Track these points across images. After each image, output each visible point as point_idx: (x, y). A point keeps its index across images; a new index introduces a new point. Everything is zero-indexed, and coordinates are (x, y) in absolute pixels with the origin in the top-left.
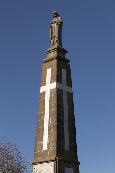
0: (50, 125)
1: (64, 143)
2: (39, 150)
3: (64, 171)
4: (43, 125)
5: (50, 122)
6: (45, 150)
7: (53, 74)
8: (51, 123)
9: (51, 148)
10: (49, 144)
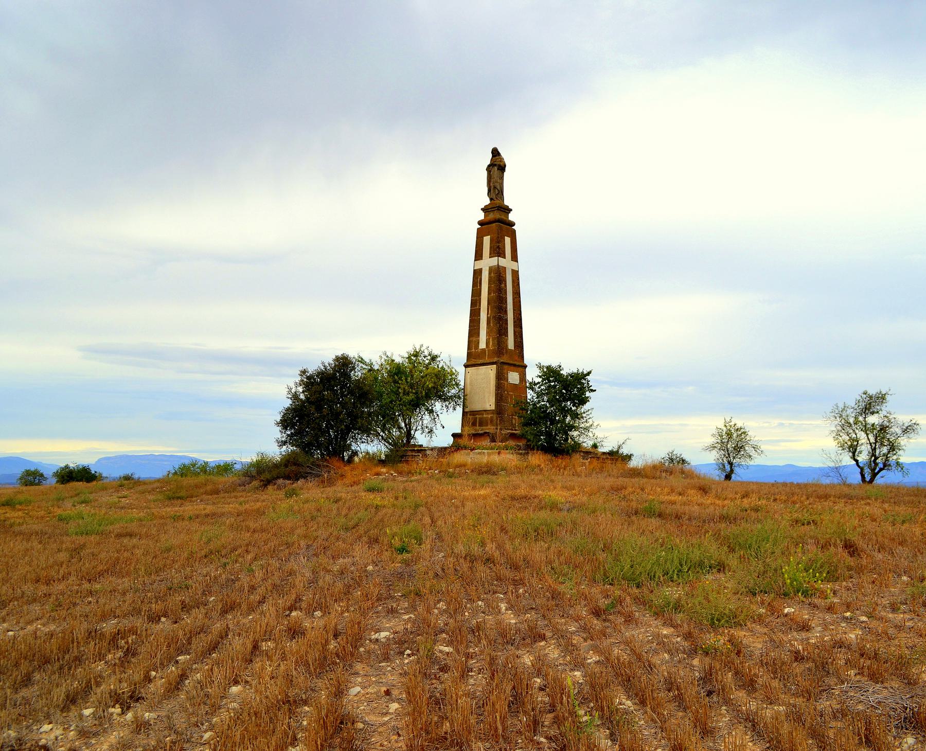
0: (489, 315)
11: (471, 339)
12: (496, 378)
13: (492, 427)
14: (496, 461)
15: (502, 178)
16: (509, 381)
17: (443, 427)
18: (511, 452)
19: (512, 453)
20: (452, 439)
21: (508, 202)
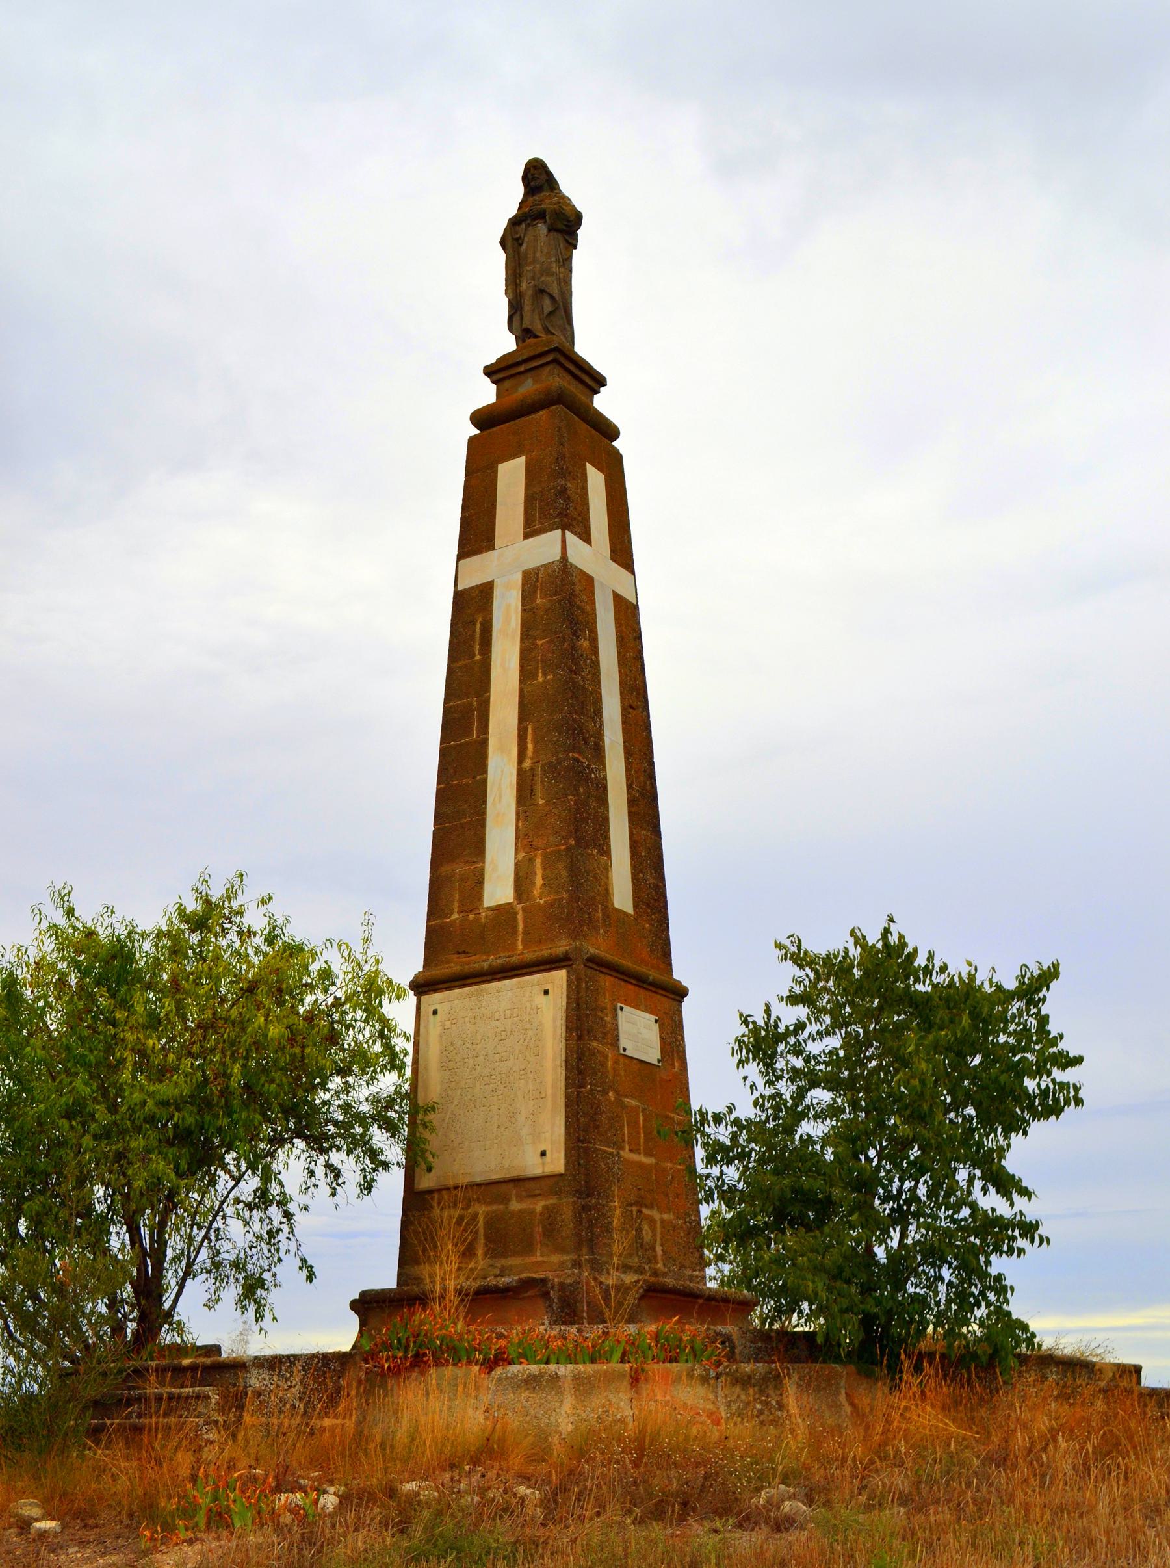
0: (527, 764)
1: (607, 868)
2: (456, 905)
3: (617, 1025)
4: (483, 769)
5: (530, 746)
6: (499, 909)
7: (537, 489)
8: (536, 751)
9: (536, 892)
10: (522, 873)
11: (445, 869)
12: (569, 1029)
13: (555, 1258)
14: (623, 1421)
15: (566, 263)
16: (623, 1043)
17: (311, 1277)
18: (699, 1371)
19: (705, 1379)
20: (354, 1321)
21: (586, 346)
